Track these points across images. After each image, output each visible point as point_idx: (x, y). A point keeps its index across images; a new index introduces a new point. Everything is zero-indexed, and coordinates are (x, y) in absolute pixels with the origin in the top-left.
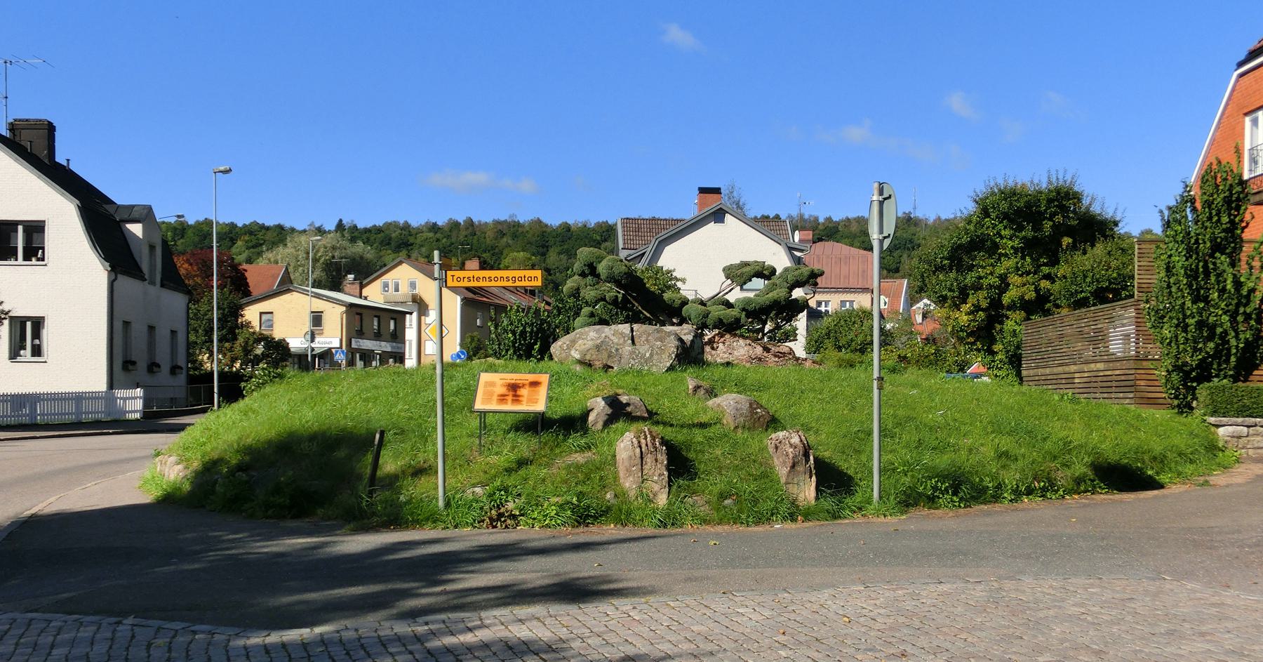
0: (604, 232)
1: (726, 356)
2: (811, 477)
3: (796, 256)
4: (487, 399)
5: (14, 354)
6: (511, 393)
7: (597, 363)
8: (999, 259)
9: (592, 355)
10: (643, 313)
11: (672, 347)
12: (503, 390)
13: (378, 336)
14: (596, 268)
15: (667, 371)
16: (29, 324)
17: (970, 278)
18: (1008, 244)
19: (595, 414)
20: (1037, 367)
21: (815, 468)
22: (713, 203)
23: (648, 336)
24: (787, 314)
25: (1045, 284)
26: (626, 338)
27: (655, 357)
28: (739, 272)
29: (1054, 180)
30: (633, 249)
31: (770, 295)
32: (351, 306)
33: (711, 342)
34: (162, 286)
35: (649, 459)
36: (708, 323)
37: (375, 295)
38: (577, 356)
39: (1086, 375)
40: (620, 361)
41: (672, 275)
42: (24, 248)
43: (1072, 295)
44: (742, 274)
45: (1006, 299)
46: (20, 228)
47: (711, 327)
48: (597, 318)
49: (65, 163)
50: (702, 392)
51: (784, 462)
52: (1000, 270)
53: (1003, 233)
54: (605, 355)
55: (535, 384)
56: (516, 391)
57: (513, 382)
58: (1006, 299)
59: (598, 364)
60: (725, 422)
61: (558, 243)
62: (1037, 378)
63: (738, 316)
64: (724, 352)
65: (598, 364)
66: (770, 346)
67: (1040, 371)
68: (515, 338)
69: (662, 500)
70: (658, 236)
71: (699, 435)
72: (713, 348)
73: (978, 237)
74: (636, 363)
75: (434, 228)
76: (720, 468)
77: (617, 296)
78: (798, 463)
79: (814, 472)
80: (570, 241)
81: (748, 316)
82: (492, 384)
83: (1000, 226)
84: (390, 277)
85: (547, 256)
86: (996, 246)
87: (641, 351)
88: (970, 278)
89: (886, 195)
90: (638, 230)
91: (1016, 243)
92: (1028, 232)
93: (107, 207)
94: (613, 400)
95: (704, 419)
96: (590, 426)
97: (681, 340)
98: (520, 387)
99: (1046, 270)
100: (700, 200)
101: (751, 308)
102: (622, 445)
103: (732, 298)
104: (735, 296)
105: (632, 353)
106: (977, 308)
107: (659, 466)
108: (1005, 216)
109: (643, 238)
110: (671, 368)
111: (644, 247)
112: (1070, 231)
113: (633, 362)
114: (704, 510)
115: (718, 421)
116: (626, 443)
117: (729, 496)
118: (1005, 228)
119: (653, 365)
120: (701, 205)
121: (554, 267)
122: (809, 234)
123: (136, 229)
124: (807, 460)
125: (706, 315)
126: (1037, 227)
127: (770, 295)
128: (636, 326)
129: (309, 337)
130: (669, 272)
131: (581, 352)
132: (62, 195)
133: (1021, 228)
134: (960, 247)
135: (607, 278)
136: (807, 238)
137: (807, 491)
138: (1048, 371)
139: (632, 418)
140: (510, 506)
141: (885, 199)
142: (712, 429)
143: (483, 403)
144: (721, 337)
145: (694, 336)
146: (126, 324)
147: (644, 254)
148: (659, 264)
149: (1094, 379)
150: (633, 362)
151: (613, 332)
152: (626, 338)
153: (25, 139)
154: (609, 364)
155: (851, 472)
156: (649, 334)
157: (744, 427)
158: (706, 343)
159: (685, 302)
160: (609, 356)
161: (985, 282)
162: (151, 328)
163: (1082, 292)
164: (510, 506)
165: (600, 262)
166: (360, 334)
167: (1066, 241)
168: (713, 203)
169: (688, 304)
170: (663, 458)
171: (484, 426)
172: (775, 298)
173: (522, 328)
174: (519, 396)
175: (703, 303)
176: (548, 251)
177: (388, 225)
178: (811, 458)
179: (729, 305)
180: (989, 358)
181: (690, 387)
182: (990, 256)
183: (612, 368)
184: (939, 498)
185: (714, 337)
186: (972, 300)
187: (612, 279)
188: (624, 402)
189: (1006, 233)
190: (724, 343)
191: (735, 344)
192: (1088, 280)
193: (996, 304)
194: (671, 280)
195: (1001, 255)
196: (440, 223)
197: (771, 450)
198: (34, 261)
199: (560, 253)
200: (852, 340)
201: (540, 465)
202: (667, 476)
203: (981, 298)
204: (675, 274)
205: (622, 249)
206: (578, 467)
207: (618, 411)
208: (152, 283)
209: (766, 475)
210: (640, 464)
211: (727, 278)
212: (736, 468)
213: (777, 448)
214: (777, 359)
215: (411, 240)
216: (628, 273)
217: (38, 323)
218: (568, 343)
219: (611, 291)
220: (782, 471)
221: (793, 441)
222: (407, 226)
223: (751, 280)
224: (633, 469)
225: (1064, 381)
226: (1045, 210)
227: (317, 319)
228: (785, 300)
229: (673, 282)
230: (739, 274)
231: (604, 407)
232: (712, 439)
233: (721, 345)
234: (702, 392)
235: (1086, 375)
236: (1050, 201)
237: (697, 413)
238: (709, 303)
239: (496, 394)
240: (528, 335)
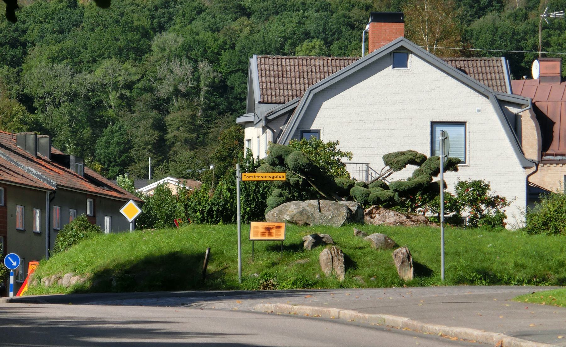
0: (156, 8)
2: (411, 268)
3: (512, 113)
4: (256, 234)
6: (267, 232)
7: (300, 222)
9: (297, 217)
10: (319, 194)
11: (344, 213)
12: (263, 230)
14: (284, 159)
15: (342, 226)
23: (329, 207)
24: (430, 195)
26: (316, 208)
27: (335, 218)
30: (276, 103)
33: (370, 213)
35: (336, 259)
36: (369, 200)
38: (288, 218)
40: (314, 221)
41: (334, 149)
44: (398, 161)
47: (371, 203)
48: (284, 198)
50: (361, 235)
51: (399, 261)
54: (305, 217)
55: (278, 227)
56: (269, 231)
57: (268, 226)
60: (372, 246)
61: (48, 36)
63: (392, 195)
64: (379, 220)
65: (301, 223)
68: (203, 217)
69: (342, 278)
70: (311, 87)
71: (359, 252)
72: (371, 217)
76: (369, 265)
77: (298, 181)
78: (405, 261)
79: (412, 265)
80: (79, 31)
82: (257, 227)
85: (24, 66)
87: (326, 215)
89: (445, 137)
95: (361, 245)
96: (305, 248)
97: (349, 209)
98: (271, 229)
101: (401, 189)
102: (323, 254)
103: (388, 181)
105: (320, 216)
107: (340, 262)
109: (289, 87)
110: (343, 225)
111: (295, 99)
114: (361, 282)
115: (369, 246)
116: (324, 254)
117: (373, 276)
119: (334, 223)
121: (40, 92)
122: (554, 67)
124: (409, 260)
125: (368, 195)
128: (321, 201)
130: (332, 145)
131: (290, 216)
135: (294, 167)
136: (550, 72)
137: (409, 274)
139: (325, 244)
140: (272, 281)
141: (445, 138)
142: (366, 249)
143: (254, 236)
144: (377, 210)
145: (358, 208)
147: (292, 112)
150: (321, 222)
152: (316, 208)
154: (308, 223)
155: (433, 269)
156: (330, 206)
157: (381, 249)
158: (367, 214)
160: (308, 218)
164: (272, 281)
165: (287, 155)
169: (354, 186)
170: (342, 259)
171: (254, 250)
172: (420, 181)
173: (209, 207)
174: (271, 233)
176: (25, 53)
178: (411, 259)
179: (385, 187)
181: (355, 232)
183: (310, 225)
184: (475, 281)
185: (372, 210)
188: (322, 236)
190: (379, 214)
191: (387, 214)
194: (334, 155)
197: (394, 257)
199: (54, 59)
201: (283, 265)
205: (260, 102)
206: (302, 265)
207: (318, 241)
209: (391, 268)
211: (386, 164)
212: (377, 265)
213: (396, 255)
214: (413, 223)
216: (310, 163)
218: (277, 212)
220: (397, 265)
221: (402, 251)
223: (405, 167)
228: (427, 183)
229: (336, 158)
230: (395, 162)
232: (366, 254)
233: (377, 215)
237: (358, 243)
238: (370, 186)
239: (260, 232)
240: (215, 213)
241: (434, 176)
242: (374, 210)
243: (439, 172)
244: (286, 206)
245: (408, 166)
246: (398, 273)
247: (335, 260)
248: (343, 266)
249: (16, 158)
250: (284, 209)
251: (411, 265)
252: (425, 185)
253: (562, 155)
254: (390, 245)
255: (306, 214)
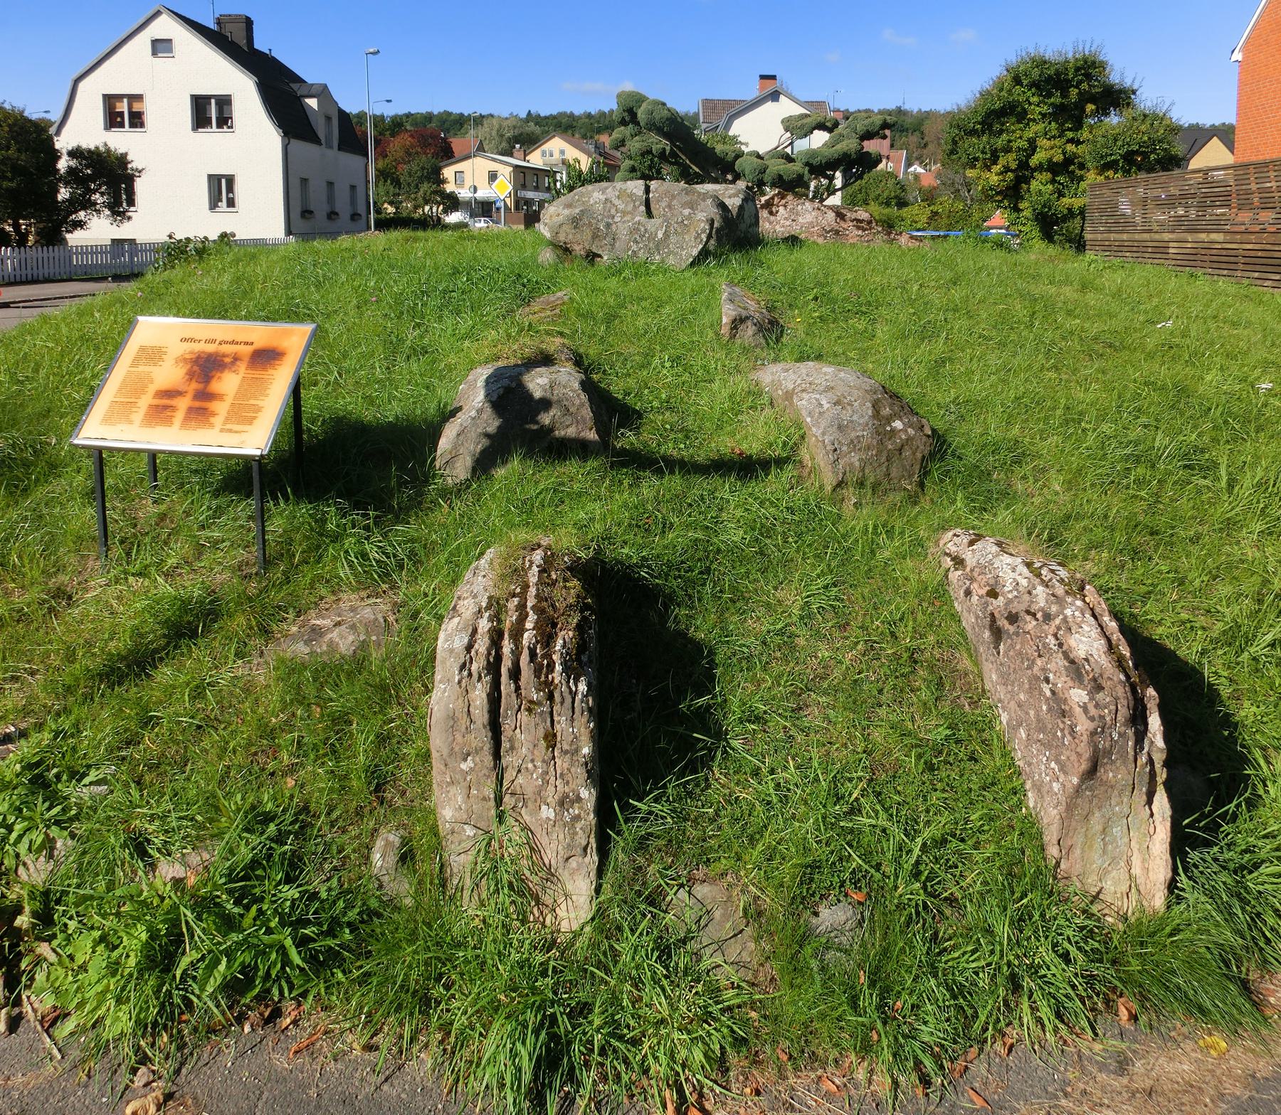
1: (788, 223)
5: (213, 205)
7: (577, 248)
8: (1028, 124)
13: (536, 189)
16: (223, 181)
17: (1000, 142)
18: (1035, 111)
19: (454, 433)
20: (1110, 232)
21: (1166, 764)
22: (771, 87)
23: (671, 201)
25: (1070, 148)
27: (673, 239)
28: (799, 124)
29: (1081, 49)
31: (838, 147)
32: (516, 167)
33: (768, 205)
34: (339, 149)
36: (765, 180)
37: (536, 159)
39: (1189, 245)
42: (217, 118)
43: (1102, 157)
45: (1034, 161)
46: (213, 101)
49: (268, 52)
50: (749, 330)
52: (1029, 134)
53: (1032, 100)
54: (588, 234)
57: (211, 348)
58: (1034, 161)
59: (578, 249)
62: (1107, 243)
63: (801, 171)
64: (786, 219)
66: (844, 211)
67: (1112, 236)
72: (771, 213)
73: (1009, 102)
74: (641, 248)
75: (589, 116)
78: (1109, 753)
79: (1162, 775)
81: (811, 172)
83: (1029, 93)
84: (547, 147)
86: (1025, 112)
88: (1000, 142)
90: (714, 108)
91: (1045, 109)
92: (1056, 99)
93: (295, 86)
94: (508, 390)
97: (722, 206)
99: (1070, 135)
100: (761, 84)
101: (815, 162)
104: (802, 145)
106: (1007, 169)
108: (1033, 84)
112: (1093, 99)
113: (635, 248)
118: (1033, 95)
120: (762, 88)
123: (313, 103)
126: (1065, 95)
127: (838, 147)
129: (472, 190)
131: (551, 229)
132: (243, 72)
133: (1049, 95)
134: (993, 112)
138: (1125, 237)
144: (782, 198)
145: (743, 200)
146: (304, 181)
148: (731, 133)
149: (1203, 252)
150: (635, 248)
151: (617, 193)
153: (228, 30)
156: (673, 197)
157: (861, 484)
158: (763, 207)
159: (739, 155)
160: (595, 236)
161: (1014, 145)
162: (330, 184)
163: (1111, 155)
166: (524, 187)
167: (1090, 107)
168: (771, 87)
175: (759, 156)
177: (561, 114)
179: (789, 159)
180: (1015, 215)
182: (1019, 122)
183: (600, 256)
186: (1002, 162)
187: (654, 127)
189: (1035, 99)
190: (785, 206)
192: (1119, 143)
193: (1023, 165)
195: (1030, 120)
196: (593, 113)
198: (225, 129)
200: (879, 195)
202: (590, 805)
203: (1010, 160)
204: (739, 139)
208: (331, 147)
210: (487, 747)
211: (787, 130)
214: (860, 232)
215: (575, 124)
217: (230, 180)
219: (659, 143)
222: (572, 115)
224: (464, 766)
225: (1150, 250)
226: (1073, 78)
227: (493, 177)
231: (480, 411)
233: (781, 209)
234: (749, 330)
235: (1189, 245)
236: (1077, 69)
238: (766, 158)
239: (152, 389)
241: (314, 334)
242: (776, 200)
243: (142, 349)
244: (582, 195)
245: (816, 132)
246: (1053, 851)
247: (521, 737)
248: (588, 795)
249: (1149, 239)
250: (578, 200)
251: (1153, 774)
252: (854, 156)
253: (6, 305)
254: (907, 453)
255: (590, 224)
